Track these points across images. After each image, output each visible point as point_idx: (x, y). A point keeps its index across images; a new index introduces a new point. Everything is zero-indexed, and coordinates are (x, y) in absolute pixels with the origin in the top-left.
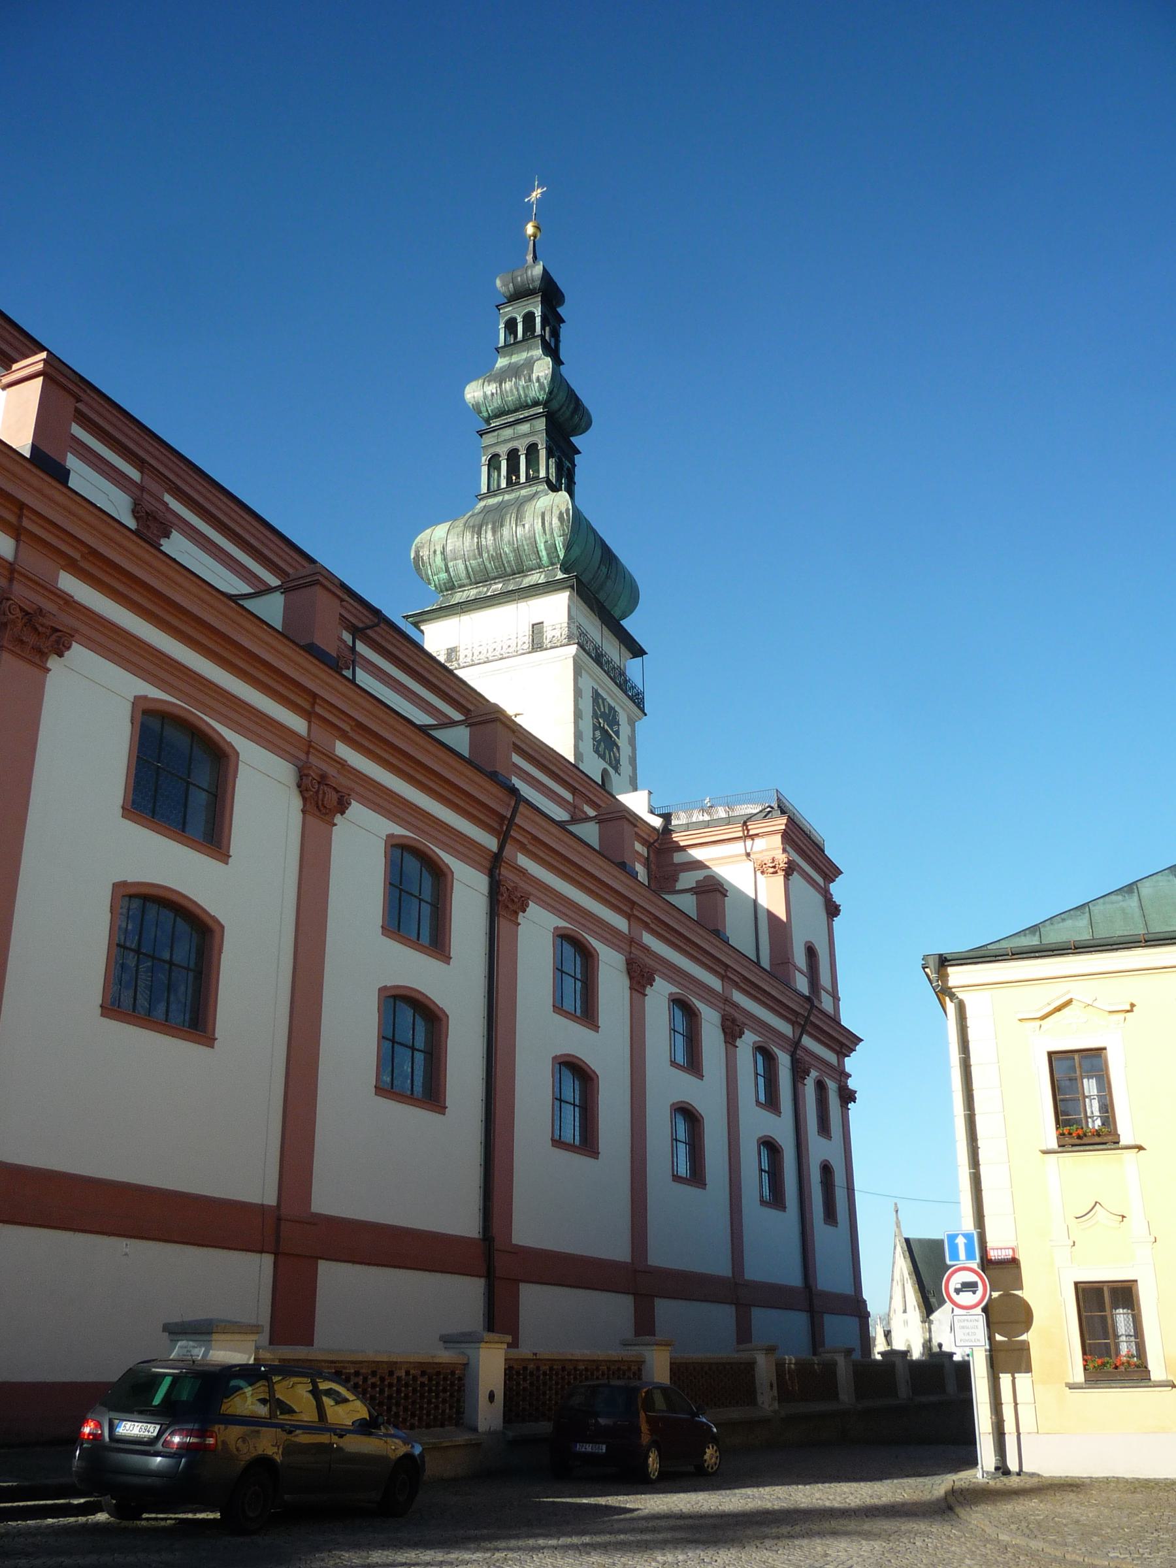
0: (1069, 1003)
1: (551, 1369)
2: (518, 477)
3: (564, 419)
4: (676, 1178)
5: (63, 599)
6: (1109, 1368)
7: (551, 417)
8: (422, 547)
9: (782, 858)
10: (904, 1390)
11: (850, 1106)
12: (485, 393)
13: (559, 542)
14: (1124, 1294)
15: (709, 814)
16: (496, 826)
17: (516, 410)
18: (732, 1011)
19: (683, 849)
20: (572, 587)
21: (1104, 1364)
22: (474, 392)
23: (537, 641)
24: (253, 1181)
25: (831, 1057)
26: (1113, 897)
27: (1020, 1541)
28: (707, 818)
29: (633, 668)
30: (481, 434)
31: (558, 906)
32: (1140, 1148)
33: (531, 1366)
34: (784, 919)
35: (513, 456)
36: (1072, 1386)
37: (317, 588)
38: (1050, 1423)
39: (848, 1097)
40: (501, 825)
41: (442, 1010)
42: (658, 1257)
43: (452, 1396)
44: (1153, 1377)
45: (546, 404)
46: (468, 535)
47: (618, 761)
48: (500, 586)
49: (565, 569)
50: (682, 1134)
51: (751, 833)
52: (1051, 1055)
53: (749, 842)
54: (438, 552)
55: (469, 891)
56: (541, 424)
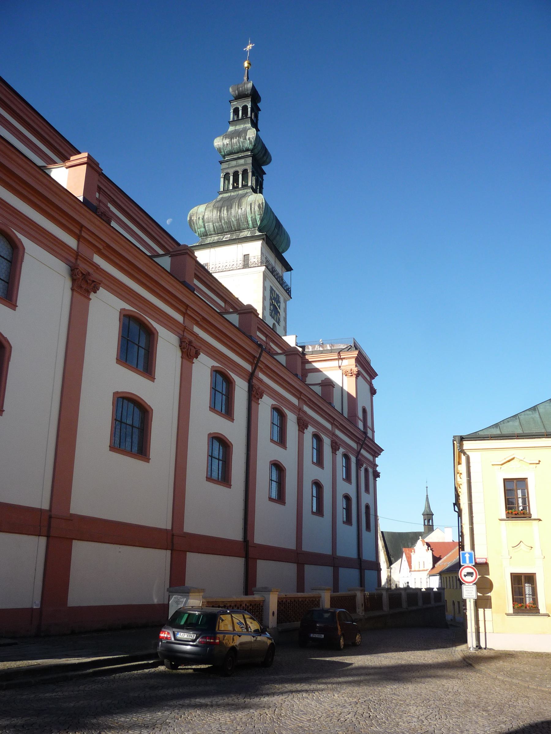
0: (513, 459)
1: (291, 601)
2: (238, 184)
3: (260, 157)
4: (271, 499)
5: (95, 266)
6: (523, 608)
7: (254, 157)
8: (193, 215)
9: (355, 370)
10: (404, 604)
11: (377, 479)
12: (223, 143)
13: (258, 218)
14: (530, 578)
15: (323, 347)
16: (251, 360)
17: (238, 153)
18: (335, 438)
19: (310, 362)
20: (263, 239)
21: (522, 606)
22: (218, 142)
23: (246, 264)
24: (162, 520)
25: (370, 457)
26: (528, 412)
27: (510, 680)
28: (321, 349)
29: (286, 276)
30: (221, 163)
31: (273, 395)
32: (540, 520)
33: (284, 600)
34: (355, 396)
35: (236, 174)
36: (508, 615)
37: (187, 256)
38: (497, 628)
39: (377, 475)
40: (254, 360)
41: (230, 442)
42: (305, 548)
43: (259, 614)
44: (541, 612)
45: (252, 151)
46: (215, 212)
47: (279, 320)
48: (229, 236)
49: (260, 231)
50: (274, 477)
51: (342, 357)
52: (504, 480)
53: (340, 361)
54: (201, 219)
55: (241, 388)
56: (250, 160)
